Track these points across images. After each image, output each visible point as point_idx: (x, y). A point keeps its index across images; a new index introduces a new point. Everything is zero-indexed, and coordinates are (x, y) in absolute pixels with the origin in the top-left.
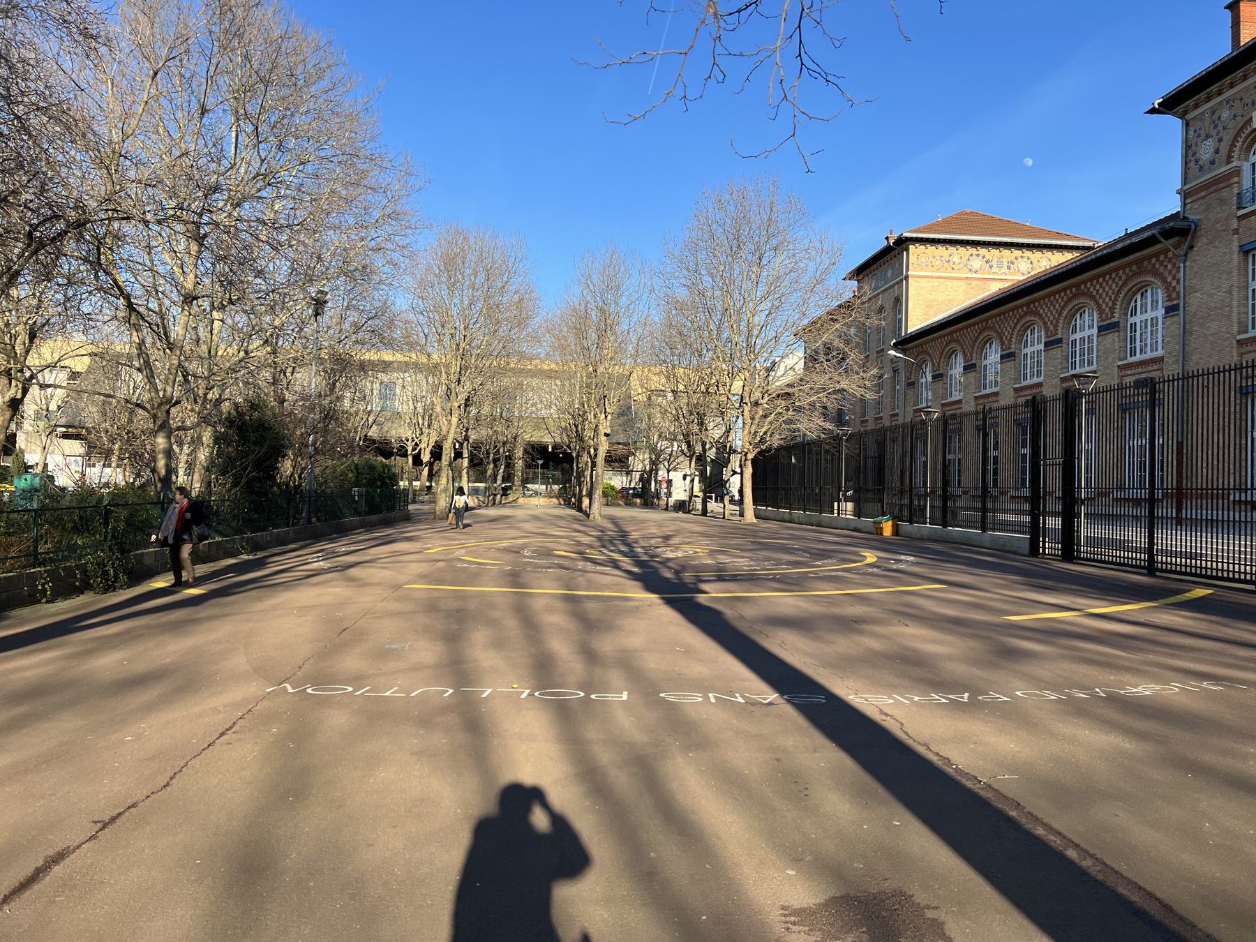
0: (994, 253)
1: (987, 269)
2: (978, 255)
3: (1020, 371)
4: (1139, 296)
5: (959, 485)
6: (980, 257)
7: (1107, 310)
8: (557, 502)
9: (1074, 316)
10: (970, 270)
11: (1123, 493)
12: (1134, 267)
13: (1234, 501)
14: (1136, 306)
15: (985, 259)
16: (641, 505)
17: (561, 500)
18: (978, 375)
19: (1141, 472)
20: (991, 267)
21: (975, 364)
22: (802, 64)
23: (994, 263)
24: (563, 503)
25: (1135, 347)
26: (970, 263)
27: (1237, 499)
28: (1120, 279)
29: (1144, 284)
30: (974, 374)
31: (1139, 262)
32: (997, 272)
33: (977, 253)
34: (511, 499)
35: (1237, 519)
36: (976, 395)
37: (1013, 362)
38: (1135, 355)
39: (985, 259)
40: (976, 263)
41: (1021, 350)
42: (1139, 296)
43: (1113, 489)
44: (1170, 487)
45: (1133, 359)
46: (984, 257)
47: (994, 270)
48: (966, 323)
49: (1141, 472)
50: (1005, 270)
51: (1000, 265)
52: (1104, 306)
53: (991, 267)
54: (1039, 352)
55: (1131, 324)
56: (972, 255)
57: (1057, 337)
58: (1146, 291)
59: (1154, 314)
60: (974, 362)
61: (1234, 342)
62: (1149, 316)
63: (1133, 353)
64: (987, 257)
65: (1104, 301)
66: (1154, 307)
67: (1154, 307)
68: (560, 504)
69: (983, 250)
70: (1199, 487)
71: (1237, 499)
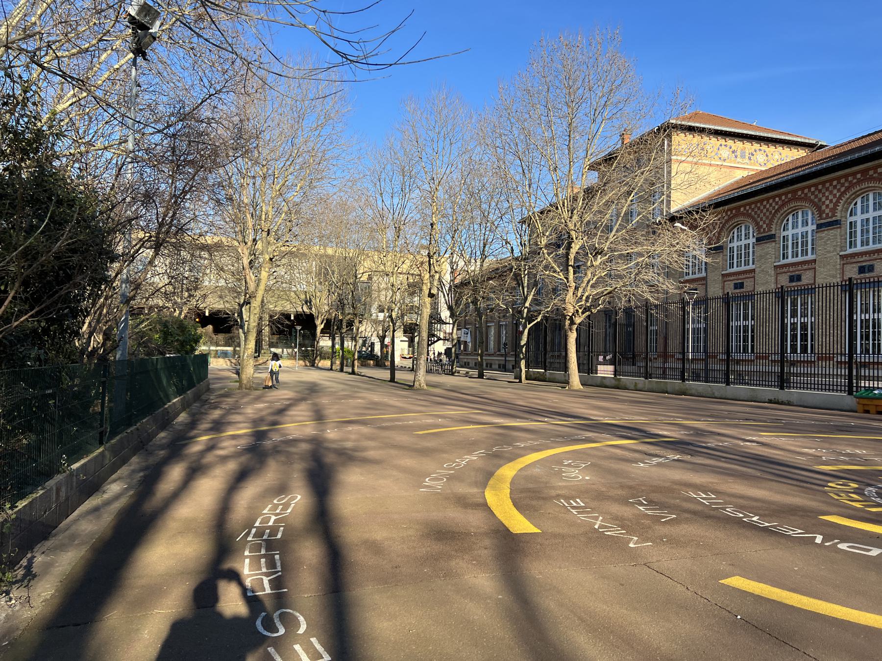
0: (738, 145)
1: (733, 159)
2: (726, 146)
3: (846, 239)
4: (859, 200)
5: (656, 349)
6: (728, 148)
7: (765, 226)
8: (303, 364)
9: (854, 199)
10: (720, 158)
11: (776, 356)
12: (859, 176)
13: (772, 360)
14: (733, 236)
15: (731, 150)
16: (374, 365)
17: (307, 362)
18: (777, 245)
19: (737, 343)
20: (736, 157)
21: (775, 235)
22: (395, 64)
23: (738, 153)
24: (308, 364)
25: (733, 263)
26: (721, 152)
27: (839, 360)
28: (843, 185)
29: (797, 208)
30: (773, 244)
31: (864, 172)
32: (740, 162)
33: (725, 143)
34: (261, 362)
35: (835, 373)
36: (775, 264)
37: (839, 230)
38: (733, 267)
39: (731, 150)
40: (725, 153)
41: (846, 218)
42: (859, 200)
43: (720, 353)
44: (831, 352)
45: (786, 261)
46: (731, 148)
47: (739, 159)
48: (761, 196)
49: (737, 343)
50: (747, 160)
51: (743, 156)
52: (761, 223)
53: (736, 157)
54: (747, 246)
55: (730, 248)
56: (721, 145)
57: (834, 219)
58: (741, 227)
59: (747, 242)
60: (773, 232)
61: (838, 257)
62: (743, 242)
63: (731, 265)
64: (733, 148)
65: (761, 220)
66: (747, 236)
67: (747, 236)
68: (306, 366)
69: (730, 141)
70: (764, 352)
71: (839, 360)
